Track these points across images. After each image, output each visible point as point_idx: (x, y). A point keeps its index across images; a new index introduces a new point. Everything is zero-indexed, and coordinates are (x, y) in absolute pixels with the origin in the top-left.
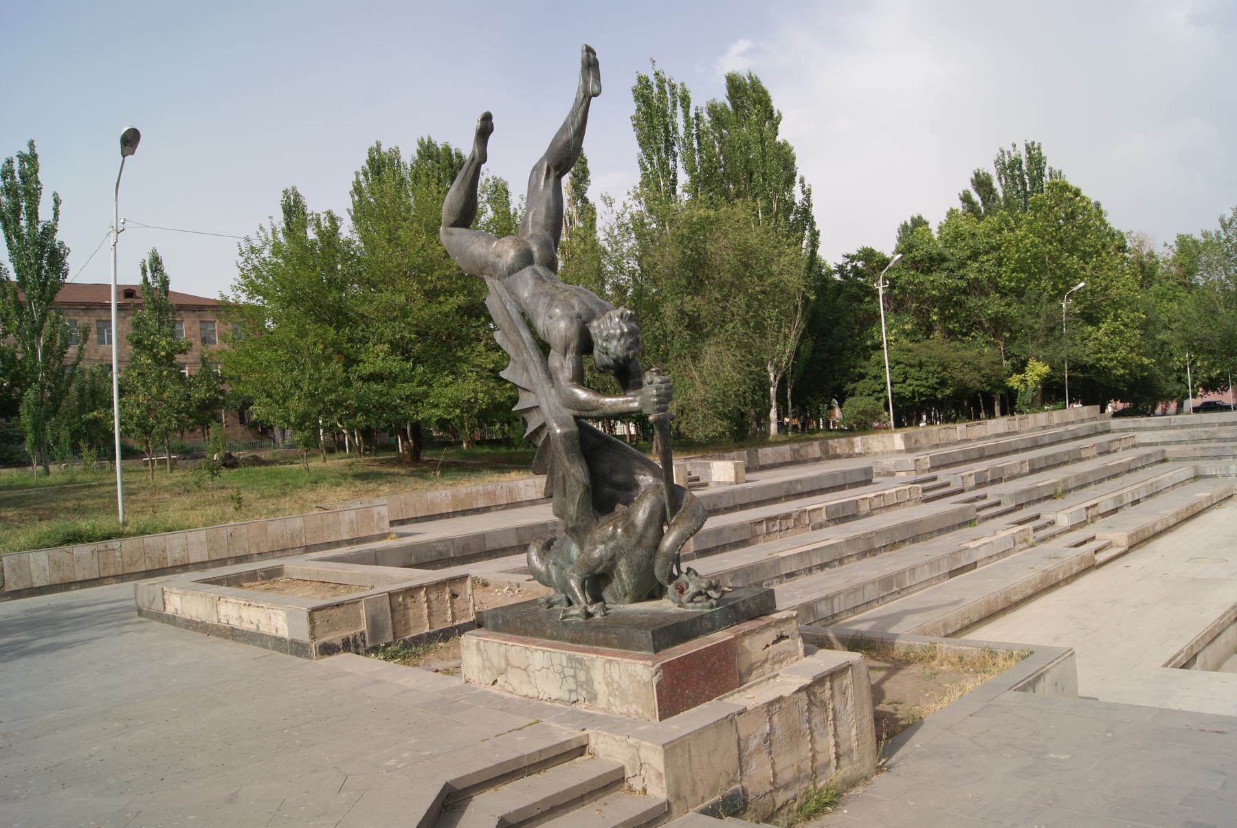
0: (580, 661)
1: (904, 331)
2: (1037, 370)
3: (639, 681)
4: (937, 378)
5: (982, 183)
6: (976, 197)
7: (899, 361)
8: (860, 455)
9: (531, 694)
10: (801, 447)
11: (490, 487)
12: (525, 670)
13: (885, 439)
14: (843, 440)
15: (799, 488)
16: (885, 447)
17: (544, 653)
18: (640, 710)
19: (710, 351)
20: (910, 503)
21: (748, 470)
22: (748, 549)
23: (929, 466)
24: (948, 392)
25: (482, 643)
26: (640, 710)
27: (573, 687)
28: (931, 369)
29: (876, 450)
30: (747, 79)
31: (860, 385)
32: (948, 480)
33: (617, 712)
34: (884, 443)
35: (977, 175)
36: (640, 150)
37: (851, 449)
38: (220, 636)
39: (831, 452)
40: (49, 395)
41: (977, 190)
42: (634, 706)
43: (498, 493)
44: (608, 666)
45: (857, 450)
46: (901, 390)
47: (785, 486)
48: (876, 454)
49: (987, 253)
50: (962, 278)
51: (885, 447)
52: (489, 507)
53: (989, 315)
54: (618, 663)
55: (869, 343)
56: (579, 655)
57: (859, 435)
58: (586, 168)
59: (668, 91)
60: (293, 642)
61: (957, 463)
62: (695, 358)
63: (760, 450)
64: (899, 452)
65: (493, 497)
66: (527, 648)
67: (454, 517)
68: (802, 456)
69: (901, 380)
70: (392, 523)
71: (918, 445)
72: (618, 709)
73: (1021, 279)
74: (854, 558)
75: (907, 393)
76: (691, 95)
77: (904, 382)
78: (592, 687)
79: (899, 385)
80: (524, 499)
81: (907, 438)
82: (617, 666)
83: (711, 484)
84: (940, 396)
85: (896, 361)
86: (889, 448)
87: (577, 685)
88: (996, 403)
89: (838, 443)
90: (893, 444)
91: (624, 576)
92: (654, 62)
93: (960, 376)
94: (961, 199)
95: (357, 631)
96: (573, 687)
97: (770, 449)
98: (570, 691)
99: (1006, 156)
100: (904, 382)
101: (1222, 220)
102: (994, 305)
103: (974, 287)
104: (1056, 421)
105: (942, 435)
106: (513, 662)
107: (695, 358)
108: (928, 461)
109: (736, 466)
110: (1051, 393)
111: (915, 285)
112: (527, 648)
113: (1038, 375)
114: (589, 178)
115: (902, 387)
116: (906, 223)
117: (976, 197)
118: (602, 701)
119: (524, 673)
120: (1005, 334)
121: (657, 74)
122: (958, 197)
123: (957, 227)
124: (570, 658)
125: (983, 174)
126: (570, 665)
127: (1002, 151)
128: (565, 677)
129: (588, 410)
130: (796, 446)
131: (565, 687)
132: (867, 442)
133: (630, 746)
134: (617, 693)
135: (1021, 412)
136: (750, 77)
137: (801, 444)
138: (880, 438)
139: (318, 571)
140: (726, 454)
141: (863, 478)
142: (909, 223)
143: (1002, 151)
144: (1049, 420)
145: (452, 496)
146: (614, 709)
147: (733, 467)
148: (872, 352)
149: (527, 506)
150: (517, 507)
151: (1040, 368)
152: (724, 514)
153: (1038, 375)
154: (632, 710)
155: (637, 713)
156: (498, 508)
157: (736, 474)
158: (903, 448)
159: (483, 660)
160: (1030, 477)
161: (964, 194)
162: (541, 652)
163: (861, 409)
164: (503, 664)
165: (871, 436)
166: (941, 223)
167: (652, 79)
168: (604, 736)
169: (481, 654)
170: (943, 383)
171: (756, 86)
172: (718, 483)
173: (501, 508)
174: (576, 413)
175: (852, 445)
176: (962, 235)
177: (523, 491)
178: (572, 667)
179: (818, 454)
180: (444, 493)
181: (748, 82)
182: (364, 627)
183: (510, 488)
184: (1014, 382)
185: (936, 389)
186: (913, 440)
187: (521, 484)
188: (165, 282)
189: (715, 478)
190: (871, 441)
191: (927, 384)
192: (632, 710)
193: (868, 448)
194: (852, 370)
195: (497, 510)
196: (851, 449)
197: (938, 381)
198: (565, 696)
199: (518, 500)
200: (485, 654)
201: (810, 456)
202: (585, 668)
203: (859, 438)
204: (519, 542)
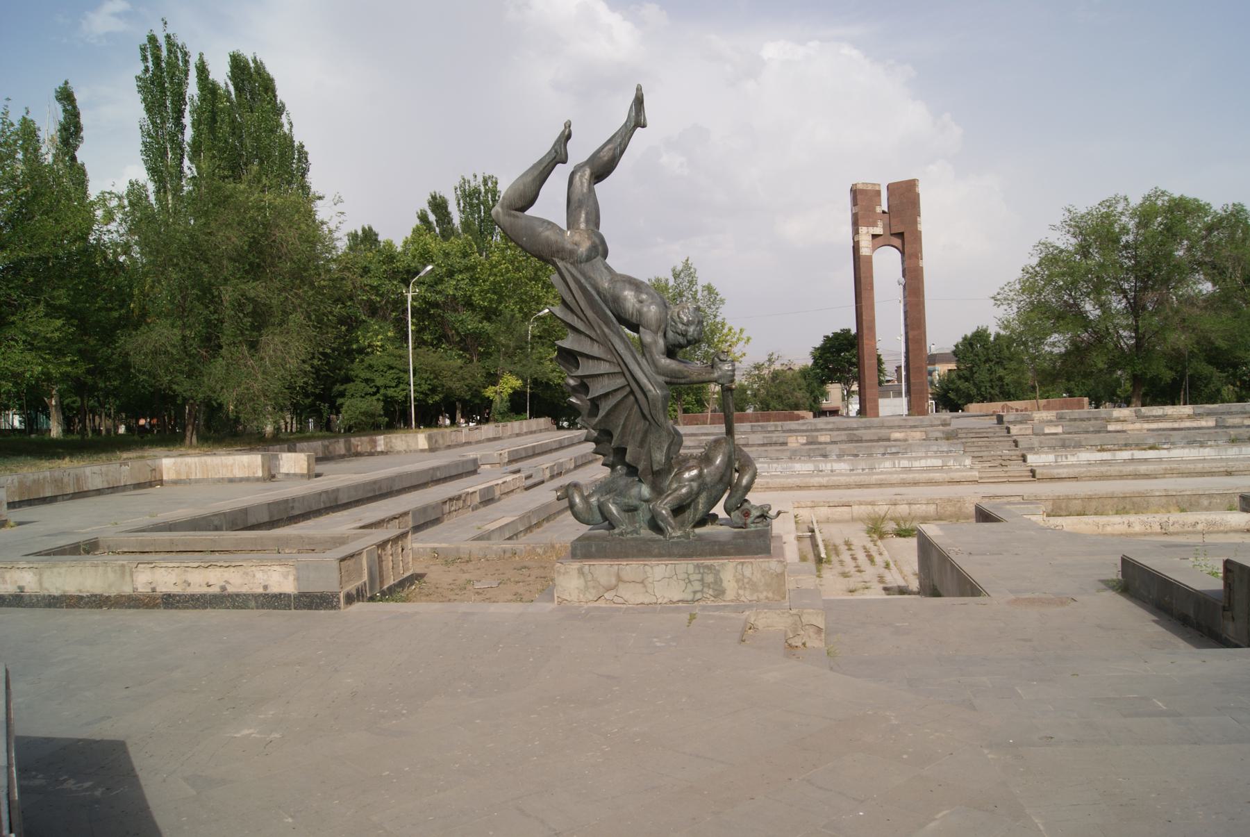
0: (709, 567)
1: (389, 339)
2: (510, 383)
3: (772, 574)
4: (429, 384)
5: (438, 205)
6: (432, 218)
7: (394, 366)
8: (382, 453)
9: (646, 601)
10: (330, 444)
11: (57, 474)
12: (642, 582)
13: (408, 439)
14: (365, 439)
15: (439, 475)
16: (408, 446)
17: (667, 565)
18: (770, 595)
19: (272, 342)
20: (518, 490)
21: (319, 460)
22: (441, 525)
23: (507, 460)
24: (437, 398)
25: (587, 567)
26: (770, 595)
27: (699, 588)
28: (425, 376)
29: (398, 448)
30: (251, 62)
31: (350, 387)
32: (531, 472)
33: (745, 600)
34: (407, 442)
35: (434, 198)
36: (144, 114)
37: (372, 448)
38: (138, 607)
39: (353, 450)
40: (359, 333)
41: (433, 211)
42: (765, 594)
43: (66, 480)
44: (739, 567)
45: (379, 449)
46: (395, 394)
47: (431, 472)
48: (399, 452)
49: (461, 272)
50: (440, 292)
51: (408, 446)
52: (56, 497)
53: (469, 330)
54: (751, 563)
55: (354, 346)
56: (708, 562)
57: (382, 434)
58: (78, 122)
59: (180, 58)
60: (302, 595)
61: (522, 458)
62: (253, 345)
63: (298, 445)
64: (423, 451)
65: (60, 485)
66: (645, 565)
67: (20, 507)
68: (330, 452)
69: (394, 384)
70: (12, 505)
71: (437, 445)
72: (747, 596)
73: (493, 299)
74: (522, 534)
75: (400, 397)
76: (209, 68)
77: (396, 386)
78: (721, 585)
79: (392, 389)
80: (91, 488)
81: (430, 438)
82: (750, 566)
83: (279, 476)
84: (431, 402)
85: (388, 365)
86: (413, 447)
87: (704, 587)
88: (458, 412)
89: (360, 441)
90: (417, 443)
91: (700, 506)
92: (166, 23)
93: (450, 384)
94: (419, 217)
95: (359, 583)
96: (699, 588)
97: (306, 444)
98: (695, 592)
99: (467, 185)
100: (397, 386)
101: (674, 270)
102: (470, 322)
103: (452, 303)
104: (525, 430)
105: (453, 437)
106: (625, 578)
107: (253, 345)
108: (506, 455)
109: (309, 457)
110: (518, 406)
111: (397, 294)
112: (645, 565)
113: (511, 388)
114: (82, 134)
115: (395, 391)
116: (356, 231)
117: (432, 218)
118: (730, 594)
119: (641, 585)
120: (480, 348)
121: (168, 37)
122: (416, 216)
123: (425, 244)
124: (697, 566)
125: (440, 197)
126: (697, 571)
127: (463, 179)
128: (690, 582)
129: (678, 378)
130: (326, 442)
131: (690, 589)
132: (391, 441)
133: (792, 615)
134: (747, 586)
135: (496, 421)
136: (255, 61)
137: (330, 440)
138: (403, 438)
139: (171, 540)
140: (271, 447)
141: (472, 468)
142: (360, 233)
143: (463, 179)
144: (521, 429)
145: (19, 482)
146: (743, 599)
147: (306, 458)
148: (356, 356)
149: (93, 496)
150: (84, 497)
151: (514, 382)
152: (396, 496)
153: (511, 388)
154: (762, 596)
155: (767, 598)
156: (65, 497)
157: (309, 465)
158: (427, 447)
159: (586, 582)
160: (575, 472)
161: (422, 213)
162: (664, 566)
163: (363, 410)
164: (614, 581)
165: (395, 435)
166: (407, 238)
167: (162, 41)
168: (765, 613)
169: (584, 576)
170: (433, 390)
171: (260, 68)
172: (287, 474)
173: (68, 497)
174: (668, 379)
175: (374, 443)
176: (429, 252)
177: (90, 480)
178: (700, 573)
179: (343, 452)
180: (10, 478)
181: (252, 65)
182: (365, 578)
183: (76, 475)
184: (489, 392)
185: (426, 395)
186: (434, 441)
187: (88, 470)
188: (600, 249)
189: (284, 470)
190: (394, 441)
191: (421, 390)
192: (762, 596)
193: (391, 447)
194: (337, 371)
195: (64, 500)
196: (372, 448)
197: (430, 387)
198: (690, 597)
199: (85, 489)
200: (589, 577)
201: (337, 453)
202: (713, 571)
203: (382, 437)
204: (271, 517)
